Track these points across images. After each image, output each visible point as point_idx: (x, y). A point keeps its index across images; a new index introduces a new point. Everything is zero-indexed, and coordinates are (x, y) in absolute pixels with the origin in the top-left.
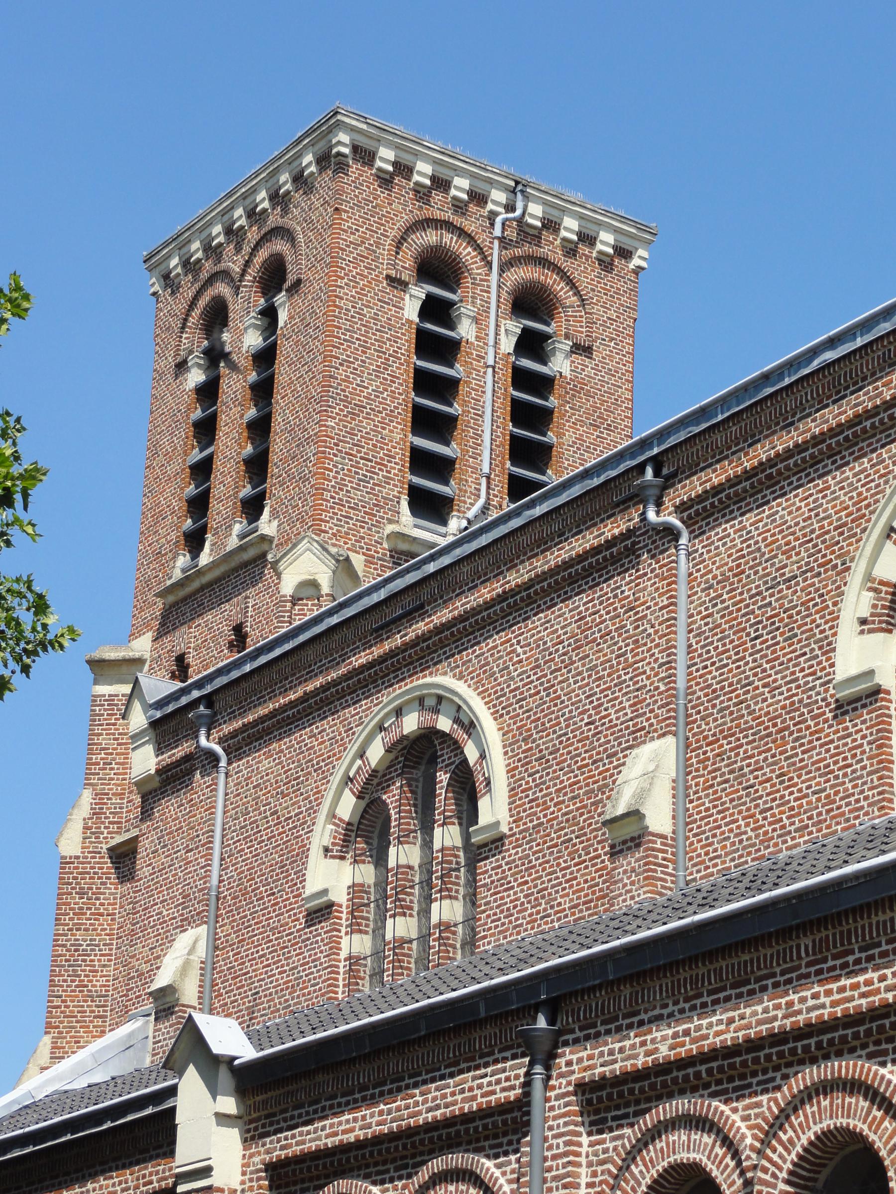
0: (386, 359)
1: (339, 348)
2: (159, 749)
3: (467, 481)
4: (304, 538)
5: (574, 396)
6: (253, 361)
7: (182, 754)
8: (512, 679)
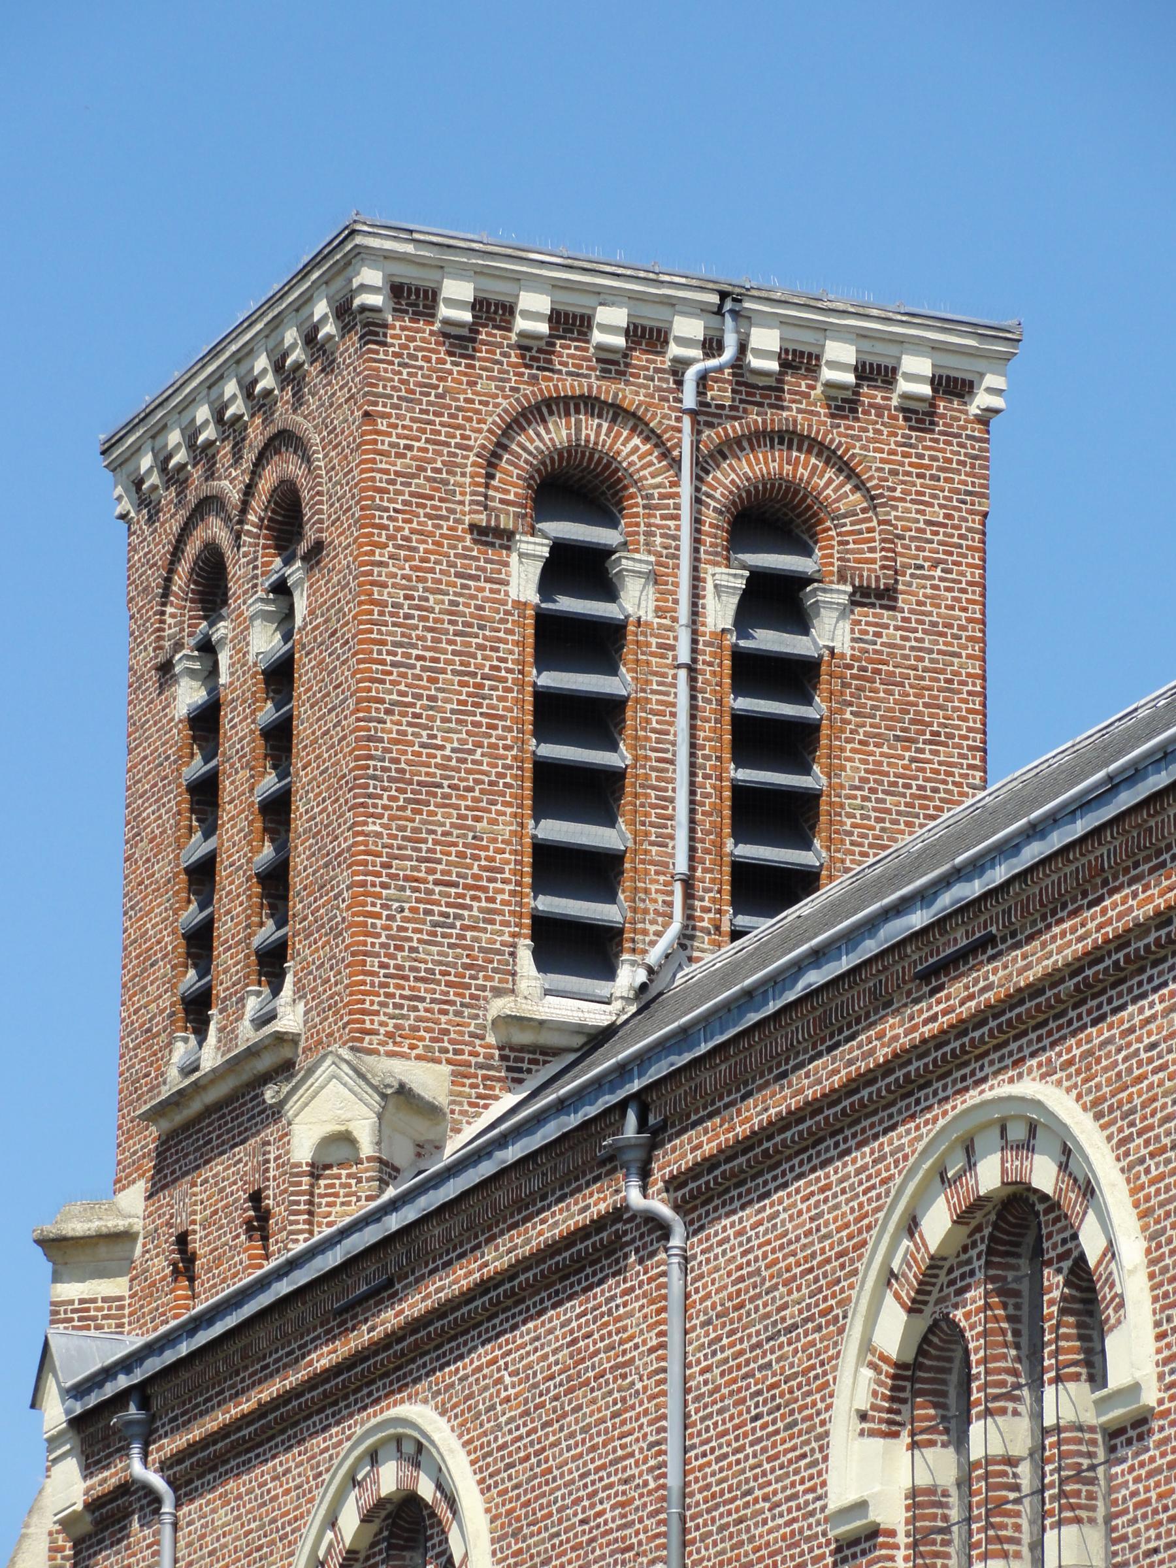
0: (476, 686)
1: (383, 682)
2: (87, 1467)
3: (646, 891)
4: (324, 1057)
5: (860, 689)
6: (267, 682)
7: (113, 1481)
8: (499, 1427)
